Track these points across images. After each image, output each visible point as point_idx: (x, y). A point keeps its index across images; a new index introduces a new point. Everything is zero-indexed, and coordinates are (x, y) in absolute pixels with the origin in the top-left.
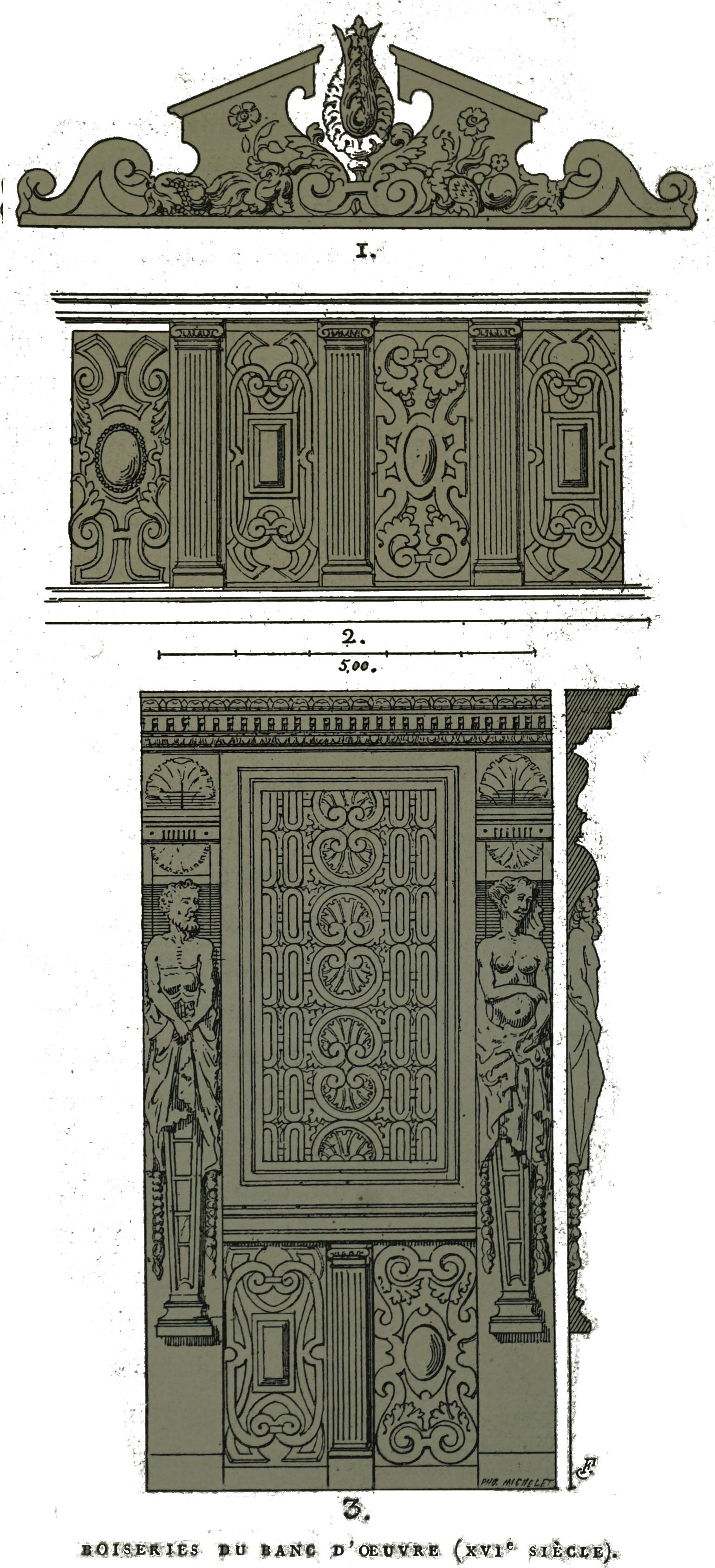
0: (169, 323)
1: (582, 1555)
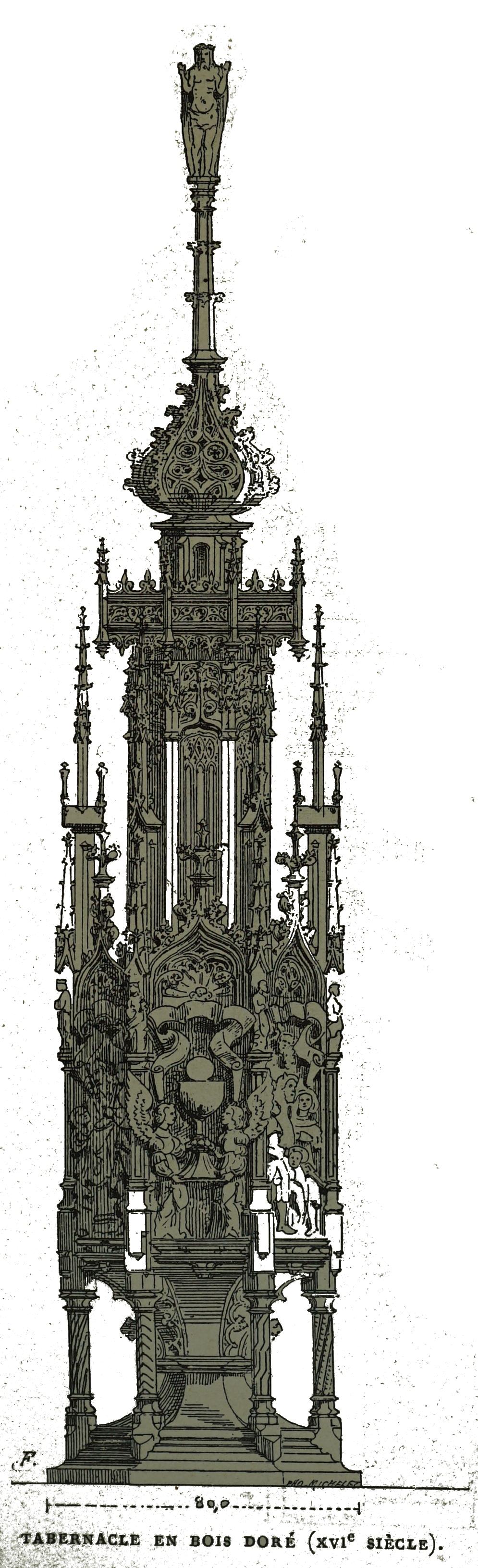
0: (252, 1191)
1: (410, 1547)
